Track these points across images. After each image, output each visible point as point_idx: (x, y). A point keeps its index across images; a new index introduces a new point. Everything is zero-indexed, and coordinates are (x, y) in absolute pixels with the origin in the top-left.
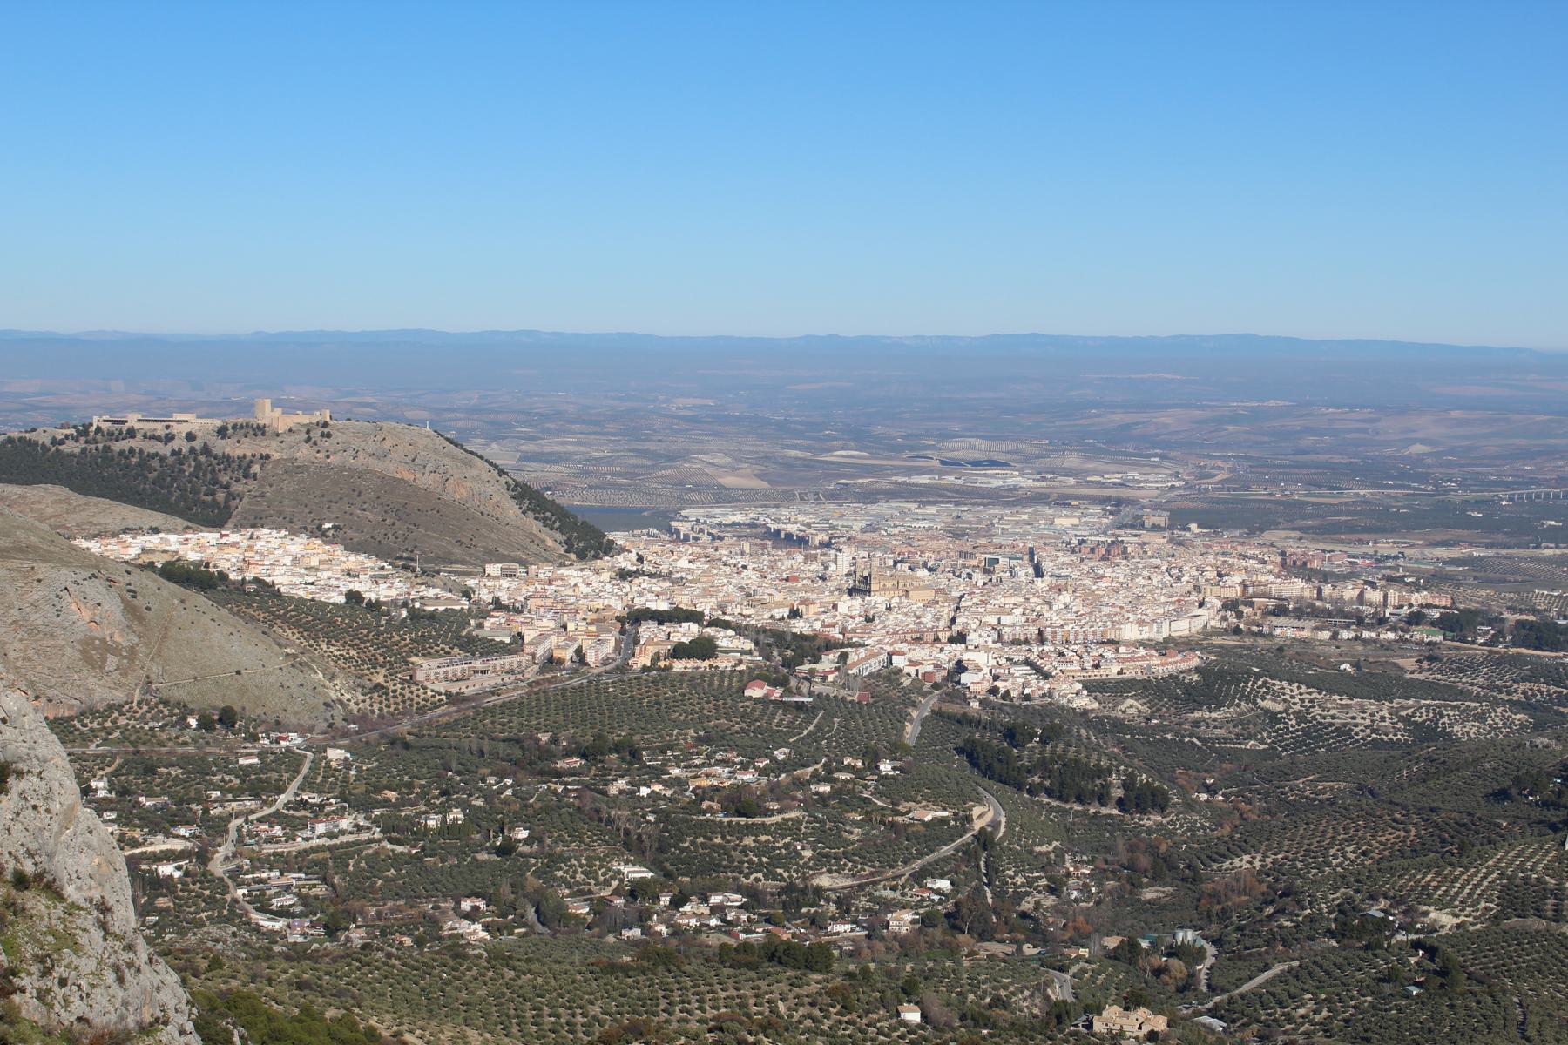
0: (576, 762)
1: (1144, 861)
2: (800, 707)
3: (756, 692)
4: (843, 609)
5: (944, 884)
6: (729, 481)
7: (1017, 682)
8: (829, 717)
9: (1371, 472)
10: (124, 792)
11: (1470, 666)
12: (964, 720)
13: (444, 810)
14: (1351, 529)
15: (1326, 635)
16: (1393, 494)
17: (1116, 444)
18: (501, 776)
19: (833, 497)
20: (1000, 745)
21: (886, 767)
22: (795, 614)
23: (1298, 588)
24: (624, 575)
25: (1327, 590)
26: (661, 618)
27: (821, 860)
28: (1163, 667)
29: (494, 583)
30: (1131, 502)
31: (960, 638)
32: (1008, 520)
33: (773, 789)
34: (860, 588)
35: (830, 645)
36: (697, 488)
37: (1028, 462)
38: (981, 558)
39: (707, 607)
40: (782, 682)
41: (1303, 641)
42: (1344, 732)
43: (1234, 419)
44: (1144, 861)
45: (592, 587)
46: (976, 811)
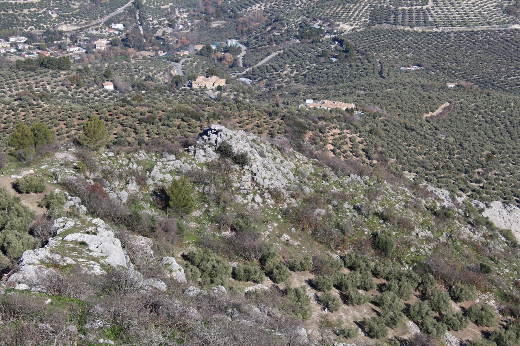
1: (212, 10)
5: (120, 26)
27: (61, 18)
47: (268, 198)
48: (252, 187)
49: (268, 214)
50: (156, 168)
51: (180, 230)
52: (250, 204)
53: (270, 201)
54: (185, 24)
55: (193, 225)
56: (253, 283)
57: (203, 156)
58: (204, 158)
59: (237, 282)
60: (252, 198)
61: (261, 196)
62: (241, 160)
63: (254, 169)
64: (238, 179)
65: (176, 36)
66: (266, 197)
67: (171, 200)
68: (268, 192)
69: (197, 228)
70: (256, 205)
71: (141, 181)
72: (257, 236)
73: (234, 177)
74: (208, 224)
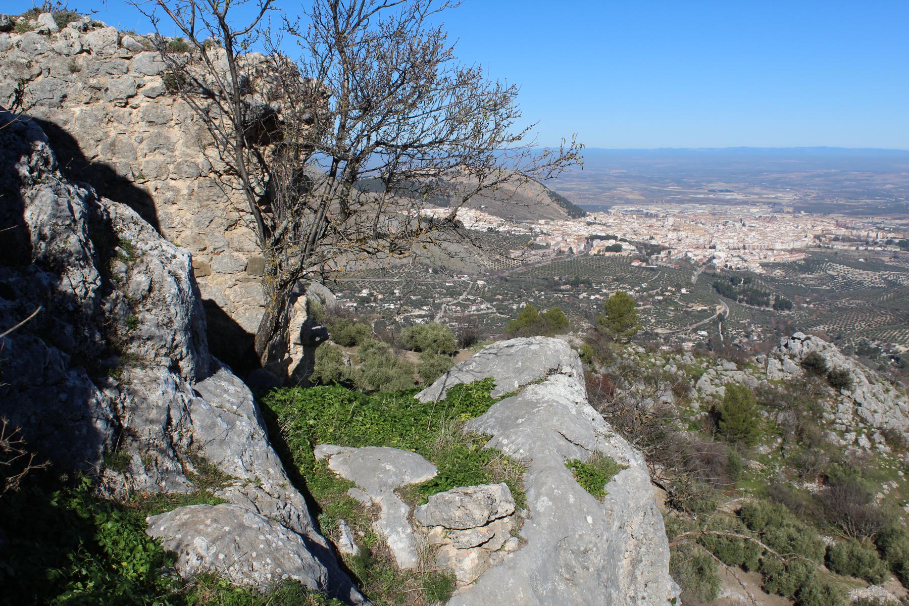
0: (568, 287)
1: (782, 327)
2: (652, 269)
4: (670, 236)
5: (704, 333)
6: (630, 197)
7: (735, 263)
8: (663, 273)
9: (871, 194)
12: (714, 275)
13: (519, 303)
14: (863, 213)
15: (854, 248)
16: (879, 202)
17: (773, 185)
18: (540, 291)
19: (668, 202)
20: (728, 284)
21: (684, 291)
22: (652, 238)
23: (842, 232)
24: (589, 224)
25: (854, 232)
27: (658, 323)
28: (788, 258)
29: (541, 226)
31: (714, 247)
32: (732, 210)
33: (642, 298)
34: (676, 229)
35: (664, 248)
36: (619, 199)
37: (740, 190)
38: (722, 221)
39: (619, 236)
40: (646, 261)
41: (846, 251)
42: (860, 283)
44: (782, 327)
45: (578, 228)
46: (718, 307)
47: (880, 443)
48: (854, 424)
49: (880, 466)
50: (705, 377)
52: (849, 447)
53: (884, 448)
54: (759, 336)
55: (755, 464)
56: (864, 582)
57: (779, 370)
58: (781, 374)
59: (834, 576)
60: (854, 438)
62: (840, 381)
63: (858, 395)
64: (832, 407)
65: (751, 345)
66: (877, 441)
67: (723, 421)
68: (881, 433)
69: (762, 471)
70: (860, 451)
71: (681, 391)
72: (868, 498)
73: (827, 405)
74: (780, 466)
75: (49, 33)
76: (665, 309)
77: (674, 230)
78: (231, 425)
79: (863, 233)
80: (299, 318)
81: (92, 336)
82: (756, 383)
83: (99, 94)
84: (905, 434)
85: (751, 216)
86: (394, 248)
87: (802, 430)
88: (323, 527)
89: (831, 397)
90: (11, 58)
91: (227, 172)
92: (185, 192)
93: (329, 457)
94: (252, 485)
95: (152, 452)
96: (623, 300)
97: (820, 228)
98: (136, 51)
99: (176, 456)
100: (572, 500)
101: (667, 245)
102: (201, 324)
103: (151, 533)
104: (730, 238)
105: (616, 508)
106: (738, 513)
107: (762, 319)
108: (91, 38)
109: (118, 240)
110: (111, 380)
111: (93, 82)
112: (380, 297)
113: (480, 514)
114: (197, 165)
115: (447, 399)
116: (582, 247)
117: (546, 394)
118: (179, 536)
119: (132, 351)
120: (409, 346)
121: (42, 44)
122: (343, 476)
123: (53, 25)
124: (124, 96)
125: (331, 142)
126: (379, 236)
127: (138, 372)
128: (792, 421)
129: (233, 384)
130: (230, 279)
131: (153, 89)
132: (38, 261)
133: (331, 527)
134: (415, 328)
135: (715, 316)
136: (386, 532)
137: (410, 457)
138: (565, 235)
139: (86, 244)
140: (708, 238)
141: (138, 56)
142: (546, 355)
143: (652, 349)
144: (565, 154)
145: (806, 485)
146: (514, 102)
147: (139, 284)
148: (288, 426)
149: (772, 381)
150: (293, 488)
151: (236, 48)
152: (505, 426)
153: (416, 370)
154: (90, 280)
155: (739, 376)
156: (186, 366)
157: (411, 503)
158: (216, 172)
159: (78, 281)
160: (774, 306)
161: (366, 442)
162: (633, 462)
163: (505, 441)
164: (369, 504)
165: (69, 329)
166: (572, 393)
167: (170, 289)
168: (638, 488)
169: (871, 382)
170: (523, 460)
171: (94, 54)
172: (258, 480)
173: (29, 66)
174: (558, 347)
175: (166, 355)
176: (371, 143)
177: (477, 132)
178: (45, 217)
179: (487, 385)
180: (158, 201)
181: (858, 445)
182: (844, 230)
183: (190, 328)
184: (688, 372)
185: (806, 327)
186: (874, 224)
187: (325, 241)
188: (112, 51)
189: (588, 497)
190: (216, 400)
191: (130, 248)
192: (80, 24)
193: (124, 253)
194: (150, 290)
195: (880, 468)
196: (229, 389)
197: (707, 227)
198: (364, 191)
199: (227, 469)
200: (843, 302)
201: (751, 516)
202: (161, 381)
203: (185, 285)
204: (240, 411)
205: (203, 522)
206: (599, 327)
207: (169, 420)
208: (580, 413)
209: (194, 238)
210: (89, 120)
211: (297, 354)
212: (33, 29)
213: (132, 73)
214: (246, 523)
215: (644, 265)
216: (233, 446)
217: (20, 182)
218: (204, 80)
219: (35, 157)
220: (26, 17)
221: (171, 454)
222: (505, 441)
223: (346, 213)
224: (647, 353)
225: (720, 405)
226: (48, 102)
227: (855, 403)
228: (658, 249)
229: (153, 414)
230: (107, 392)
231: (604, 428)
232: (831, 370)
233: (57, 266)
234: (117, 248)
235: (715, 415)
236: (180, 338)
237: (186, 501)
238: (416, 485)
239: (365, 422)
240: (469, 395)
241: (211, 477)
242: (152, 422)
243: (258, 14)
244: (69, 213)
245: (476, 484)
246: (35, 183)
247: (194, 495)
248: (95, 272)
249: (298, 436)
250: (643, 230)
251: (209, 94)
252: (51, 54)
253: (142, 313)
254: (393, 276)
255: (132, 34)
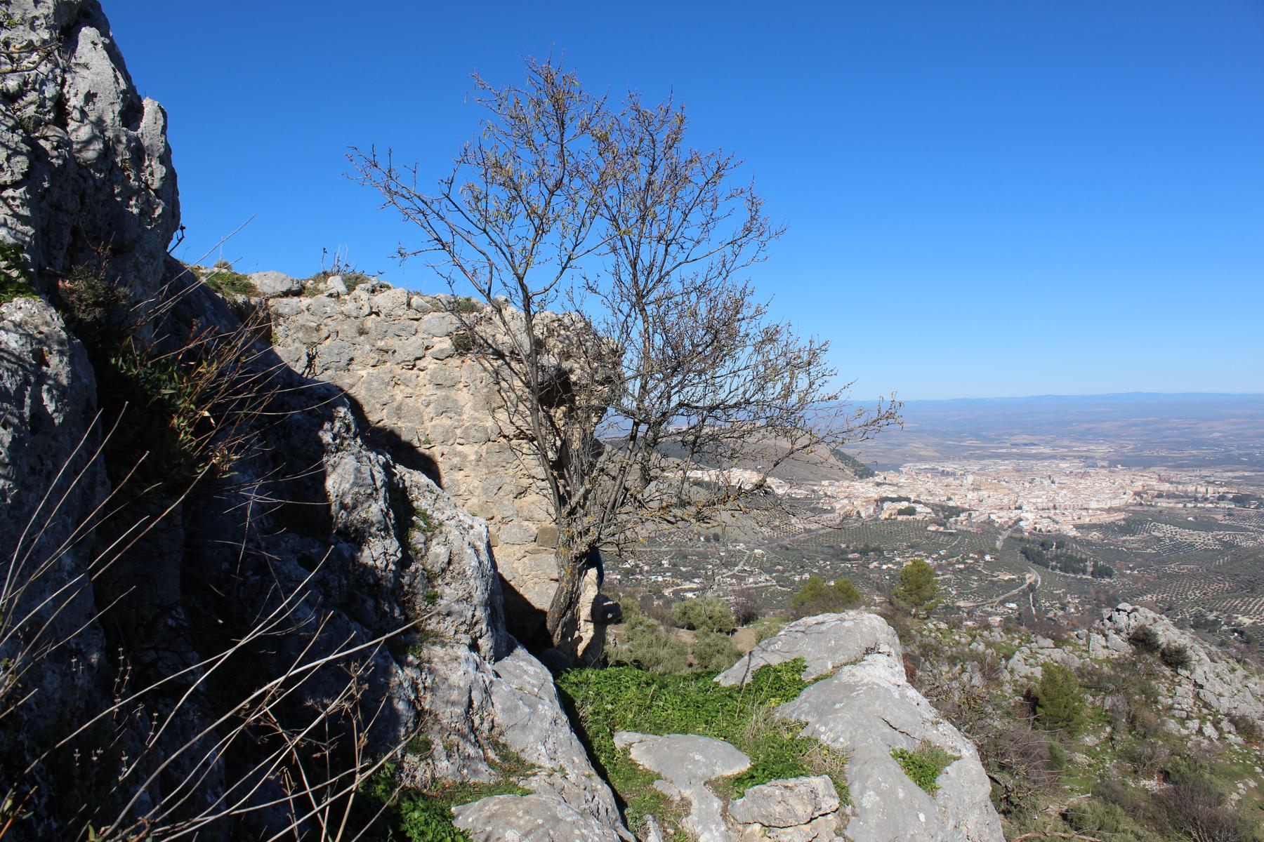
0: (857, 555)
1: (1103, 597)
2: (951, 534)
3: (932, 528)
4: (969, 497)
5: (1013, 605)
6: (923, 453)
7: (1045, 525)
8: (964, 538)
9: (1197, 444)
10: (675, 565)
11: (1249, 518)
12: (1022, 539)
13: (801, 574)
14: (1189, 466)
15: (1181, 505)
16: (1206, 452)
17: (1083, 436)
18: (825, 560)
19: (965, 458)
20: (1037, 549)
21: (988, 558)
22: (949, 499)
23: (1166, 487)
24: (878, 484)
25: (1180, 487)
26: (893, 500)
27: (960, 595)
28: (1106, 518)
29: (826, 487)
30: (1092, 458)
31: (1020, 508)
32: (1039, 465)
33: (940, 567)
34: (976, 489)
35: (964, 510)
36: (911, 456)
37: (1046, 443)
38: (1028, 478)
39: (913, 497)
40: (944, 525)
41: (1172, 508)
42: (1191, 545)
43: (1136, 425)
44: (1103, 597)
45: (865, 489)
46: (1028, 576)
47: (1230, 732)
48: (1196, 709)
49: (1231, 760)
50: (1018, 656)
51: (1054, 762)
53: (1235, 739)
54: (1076, 608)
55: (1081, 758)
58: (1106, 652)
60: (1197, 726)
61: (1215, 726)
62: (1176, 659)
63: (1199, 676)
66: (1226, 730)
67: (1041, 706)
70: (1206, 742)
71: (991, 673)
72: (1220, 799)
73: (1162, 687)
74: (1111, 760)
75: (338, 295)
76: (968, 579)
77: (974, 490)
78: (533, 707)
79: (1191, 488)
80: (589, 593)
81: (392, 610)
82: (1077, 663)
83: (386, 357)
84: (1259, 722)
85: (1062, 472)
86: (700, 518)
87: (1134, 717)
88: (630, 822)
89: (1166, 678)
90: (301, 322)
91: (517, 437)
92: (473, 457)
93: (630, 745)
94: (558, 775)
95: (452, 737)
96: (921, 569)
97: (1140, 483)
98: (425, 312)
99: (477, 741)
100: (901, 795)
101: (967, 506)
102: (499, 599)
103: (459, 824)
104: (1038, 497)
105: (950, 804)
106: (1064, 816)
107: (1080, 589)
108: (381, 300)
109: (414, 509)
110: (411, 658)
111: (381, 344)
112: (646, 568)
113: (804, 810)
114: (485, 429)
115: (754, 682)
116: (871, 511)
117: (863, 678)
118: (489, 829)
119: (431, 627)
120: (681, 623)
121: (331, 306)
122: (647, 767)
123: (341, 288)
124: (412, 358)
125: (627, 402)
126: (683, 504)
127: (438, 650)
128: (1122, 706)
129: (531, 663)
130: (518, 551)
131: (442, 351)
132: (339, 532)
133: (639, 823)
134: (687, 603)
135: (1024, 586)
136: (698, 829)
137: (718, 745)
138: (853, 497)
139: (387, 514)
140: (1013, 497)
141: (426, 318)
142: (861, 632)
143: (955, 625)
144: (883, 412)
145: (1144, 782)
146: (823, 358)
147: (437, 556)
148: (586, 711)
149: (1095, 660)
150: (599, 779)
151: (534, 308)
152: (822, 712)
153: (690, 650)
154: (391, 551)
155: (1058, 654)
156: (485, 644)
157: (725, 797)
158: (505, 437)
159: (378, 552)
160: (1092, 574)
161: (669, 730)
162: (965, 753)
163: (823, 729)
164: (677, 798)
165: (370, 603)
166: (893, 675)
167: (469, 562)
168: (973, 782)
169: (1213, 660)
170: (846, 749)
171: (382, 316)
172: (562, 769)
173: (318, 329)
174: (868, 623)
175: (466, 632)
176: (673, 404)
177: (788, 391)
178: (348, 486)
179: (797, 666)
180: (443, 467)
181: (1203, 734)
182: (1168, 485)
183: (489, 604)
184: (998, 651)
185: (1131, 596)
186: (1202, 477)
187: (623, 510)
188: (400, 313)
189: (919, 792)
190: (516, 681)
191: (426, 517)
192: (369, 286)
193: (422, 523)
194: (449, 563)
195: (1232, 763)
196: (526, 669)
197: (1012, 486)
198: (665, 456)
199: (529, 757)
200: (1173, 567)
201: (1080, 819)
202: (462, 660)
203: (484, 557)
204: (542, 695)
205: (514, 814)
206: (895, 599)
207: (471, 702)
208: (903, 697)
209: (481, 506)
210: (375, 384)
211: (587, 632)
212: (322, 292)
213: (420, 335)
214: (560, 816)
215: (942, 529)
216: (536, 732)
217: (322, 449)
218: (494, 340)
219: (338, 424)
220: (315, 280)
221: (472, 737)
222: (823, 729)
223: (647, 479)
224: (950, 629)
225: (1037, 688)
226: (334, 365)
227: (1196, 684)
228: (956, 511)
229: (455, 695)
230: (408, 671)
231: (930, 713)
232: (1164, 646)
233: (357, 537)
234: (414, 518)
235: (1032, 701)
236: (480, 613)
237: (491, 790)
238: (728, 778)
239: (667, 706)
240: (778, 677)
241: (513, 765)
242: (453, 704)
243: (558, 273)
244: (371, 481)
245: (796, 776)
246: (338, 450)
247: (498, 784)
248: (396, 544)
249: (596, 722)
250: (939, 490)
251: (500, 355)
252: (341, 317)
253: (440, 587)
254: (661, 545)
255: (418, 294)
